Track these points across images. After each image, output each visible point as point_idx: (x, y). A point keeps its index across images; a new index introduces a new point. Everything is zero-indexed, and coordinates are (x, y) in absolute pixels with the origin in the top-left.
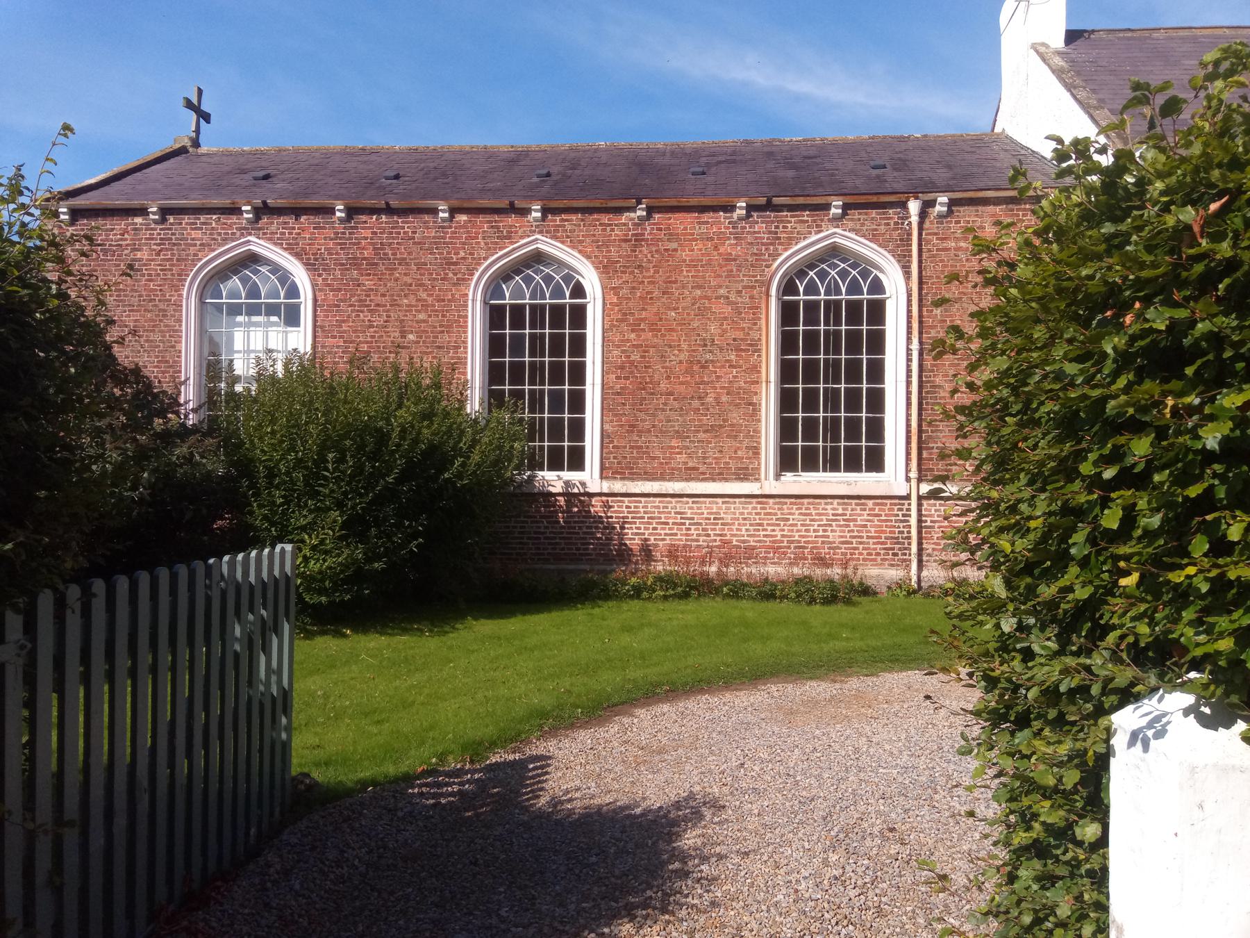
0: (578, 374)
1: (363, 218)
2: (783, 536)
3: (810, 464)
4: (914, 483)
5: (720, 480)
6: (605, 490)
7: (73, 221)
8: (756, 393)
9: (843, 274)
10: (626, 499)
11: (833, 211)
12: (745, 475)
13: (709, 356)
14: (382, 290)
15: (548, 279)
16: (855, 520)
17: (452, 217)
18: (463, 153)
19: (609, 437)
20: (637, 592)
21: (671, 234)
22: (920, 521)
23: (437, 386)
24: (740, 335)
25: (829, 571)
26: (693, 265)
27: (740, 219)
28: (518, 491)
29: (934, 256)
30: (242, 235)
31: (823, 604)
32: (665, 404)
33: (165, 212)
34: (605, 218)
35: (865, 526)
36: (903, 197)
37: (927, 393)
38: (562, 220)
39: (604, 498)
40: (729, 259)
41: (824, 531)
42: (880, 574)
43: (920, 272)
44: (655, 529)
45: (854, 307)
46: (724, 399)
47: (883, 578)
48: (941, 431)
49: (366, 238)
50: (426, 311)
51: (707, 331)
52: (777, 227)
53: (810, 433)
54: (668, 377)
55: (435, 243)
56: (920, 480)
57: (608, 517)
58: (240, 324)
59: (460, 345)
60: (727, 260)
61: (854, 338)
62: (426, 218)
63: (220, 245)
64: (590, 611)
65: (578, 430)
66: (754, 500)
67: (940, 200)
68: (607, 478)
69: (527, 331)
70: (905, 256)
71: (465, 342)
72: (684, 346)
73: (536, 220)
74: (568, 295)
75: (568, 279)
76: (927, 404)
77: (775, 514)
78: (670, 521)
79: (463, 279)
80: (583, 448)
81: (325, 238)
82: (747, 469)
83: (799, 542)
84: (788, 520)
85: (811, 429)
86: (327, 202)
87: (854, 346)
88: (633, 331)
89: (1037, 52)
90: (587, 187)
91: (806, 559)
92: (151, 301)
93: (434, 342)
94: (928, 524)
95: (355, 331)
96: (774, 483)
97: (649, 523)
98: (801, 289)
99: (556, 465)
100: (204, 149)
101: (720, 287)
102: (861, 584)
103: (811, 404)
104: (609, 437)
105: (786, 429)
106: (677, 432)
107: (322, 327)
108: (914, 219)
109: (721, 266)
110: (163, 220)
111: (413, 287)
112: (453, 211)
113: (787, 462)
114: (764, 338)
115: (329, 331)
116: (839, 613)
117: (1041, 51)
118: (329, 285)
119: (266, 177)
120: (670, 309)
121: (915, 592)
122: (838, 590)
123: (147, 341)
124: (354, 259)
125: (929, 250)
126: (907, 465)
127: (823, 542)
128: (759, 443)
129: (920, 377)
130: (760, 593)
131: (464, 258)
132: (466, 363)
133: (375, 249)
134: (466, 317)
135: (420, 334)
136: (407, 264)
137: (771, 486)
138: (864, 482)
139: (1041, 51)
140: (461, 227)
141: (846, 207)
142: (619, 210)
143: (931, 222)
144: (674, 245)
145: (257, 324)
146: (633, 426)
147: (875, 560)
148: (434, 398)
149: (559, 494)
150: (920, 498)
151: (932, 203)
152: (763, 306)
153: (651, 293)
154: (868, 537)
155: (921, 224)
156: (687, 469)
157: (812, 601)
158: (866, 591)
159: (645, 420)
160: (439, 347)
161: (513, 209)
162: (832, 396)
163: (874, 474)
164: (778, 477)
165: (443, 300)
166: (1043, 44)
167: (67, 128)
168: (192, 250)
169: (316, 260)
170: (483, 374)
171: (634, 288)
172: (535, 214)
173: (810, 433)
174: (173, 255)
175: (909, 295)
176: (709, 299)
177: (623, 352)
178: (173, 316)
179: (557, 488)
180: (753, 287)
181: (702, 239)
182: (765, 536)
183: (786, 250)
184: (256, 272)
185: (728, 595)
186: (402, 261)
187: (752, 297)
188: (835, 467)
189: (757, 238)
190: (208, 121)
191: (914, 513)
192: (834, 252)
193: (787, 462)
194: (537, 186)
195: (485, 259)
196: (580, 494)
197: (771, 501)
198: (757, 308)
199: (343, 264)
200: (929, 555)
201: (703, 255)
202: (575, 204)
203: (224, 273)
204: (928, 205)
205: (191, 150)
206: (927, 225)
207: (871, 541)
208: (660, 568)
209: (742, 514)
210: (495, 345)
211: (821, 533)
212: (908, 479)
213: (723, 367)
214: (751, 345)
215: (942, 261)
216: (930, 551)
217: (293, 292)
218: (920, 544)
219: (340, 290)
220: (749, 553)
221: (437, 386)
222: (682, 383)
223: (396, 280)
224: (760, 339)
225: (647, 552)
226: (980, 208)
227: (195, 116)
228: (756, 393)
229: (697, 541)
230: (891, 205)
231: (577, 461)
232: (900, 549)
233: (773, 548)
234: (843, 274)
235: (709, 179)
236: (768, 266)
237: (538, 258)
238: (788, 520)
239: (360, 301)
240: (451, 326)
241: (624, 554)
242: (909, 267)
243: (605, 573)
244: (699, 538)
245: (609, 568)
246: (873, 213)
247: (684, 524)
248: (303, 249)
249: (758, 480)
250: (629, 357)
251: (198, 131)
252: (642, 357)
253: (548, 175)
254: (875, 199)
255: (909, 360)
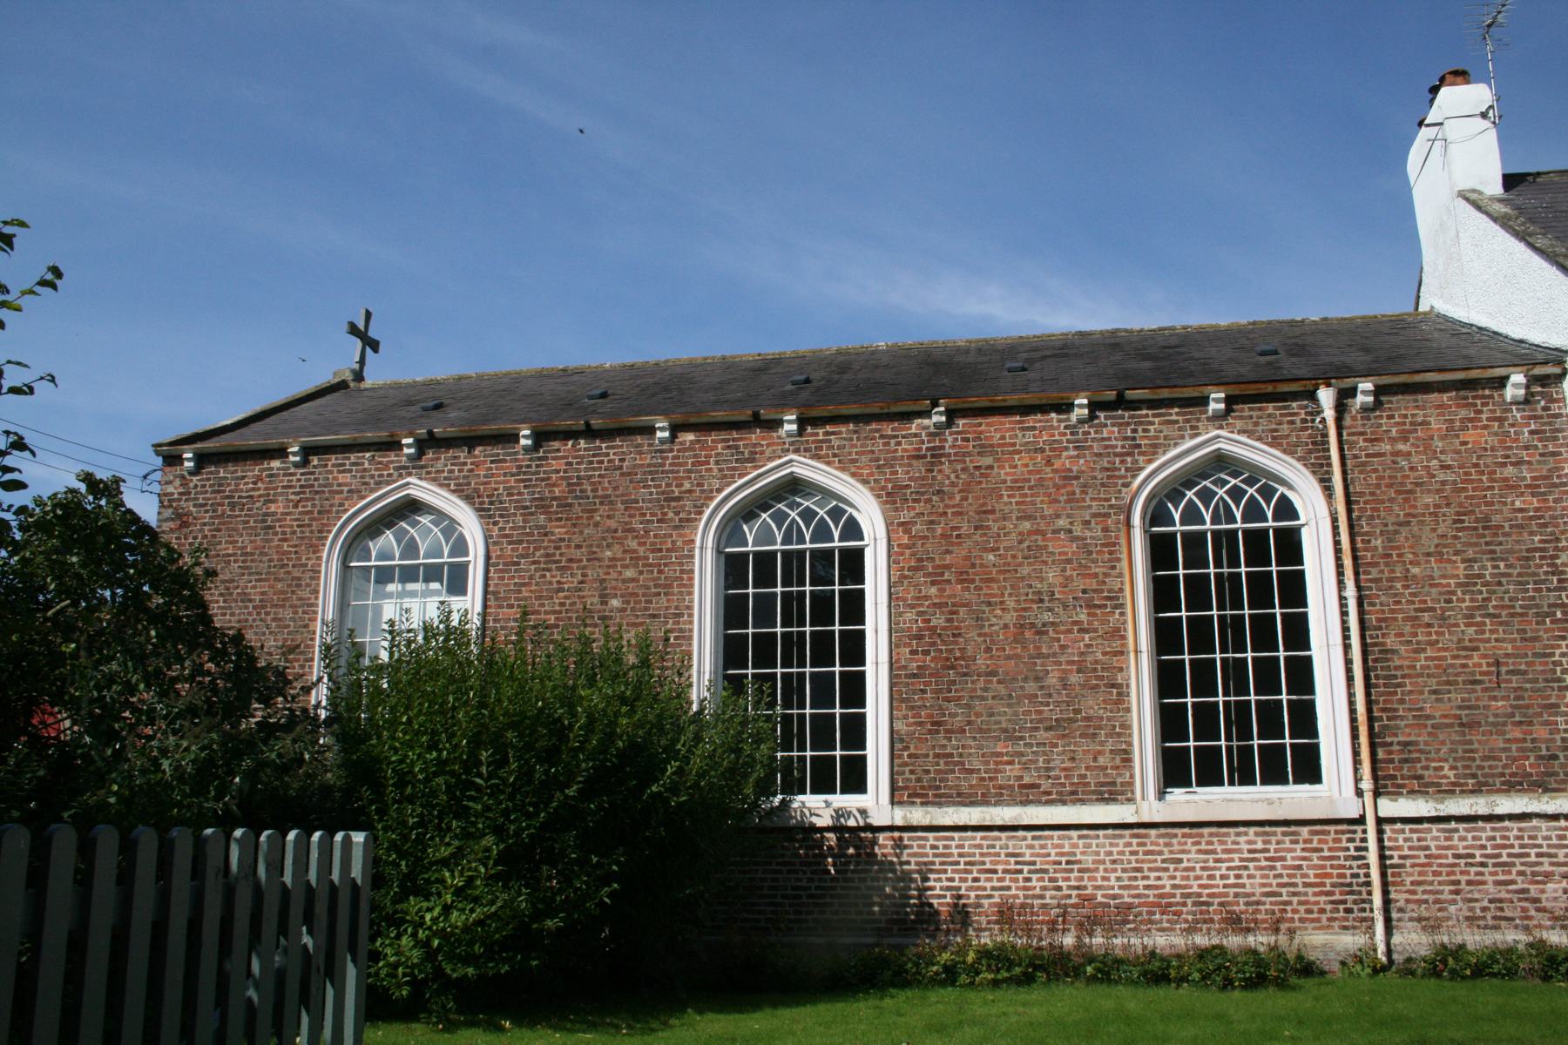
0: (855, 649)
1: (556, 444)
2: (1174, 887)
3: (1210, 777)
4: (1368, 797)
5: (1074, 802)
6: (899, 822)
7: (197, 471)
8: (1121, 670)
9: (1236, 494)
10: (930, 835)
11: (1213, 406)
12: (1113, 792)
13: (1047, 617)
14: (577, 539)
15: (808, 515)
16: (1283, 859)
17: (673, 436)
18: (692, 365)
19: (902, 740)
20: (950, 975)
21: (982, 446)
22: (1382, 857)
23: (645, 663)
24: (1092, 584)
25: (1251, 939)
26: (1017, 486)
27: (1081, 422)
28: (767, 823)
29: (1364, 464)
30: (401, 476)
31: (1244, 988)
32: (985, 690)
33: (308, 451)
34: (888, 428)
35: (1299, 867)
36: (1309, 385)
37: (1375, 661)
38: (827, 433)
39: (896, 834)
40: (1068, 477)
41: (1238, 877)
42: (1329, 942)
43: (1346, 487)
44: (976, 880)
45: (1256, 541)
46: (1074, 679)
47: (1332, 948)
48: (1402, 718)
49: (558, 472)
50: (636, 566)
51: (1042, 579)
52: (1134, 431)
53: (1207, 727)
54: (988, 650)
55: (650, 473)
56: (1377, 794)
57: (902, 863)
58: (390, 596)
59: (682, 612)
60: (1066, 478)
61: (1260, 584)
62: (639, 440)
63: (373, 491)
64: (877, 1002)
65: (855, 731)
66: (1127, 832)
67: (1361, 386)
68: (901, 803)
69: (779, 589)
70: (1322, 465)
71: (690, 608)
72: (1010, 603)
73: (789, 435)
74: (836, 535)
75: (836, 514)
76: (1377, 677)
77: (1160, 853)
78: (1000, 867)
79: (688, 520)
80: (863, 758)
81: (505, 475)
82: (1114, 784)
83: (1200, 895)
84: (1180, 861)
85: (1207, 721)
86: (507, 426)
87: (1261, 594)
88: (933, 583)
89: (1467, 199)
90: (855, 393)
91: (1212, 921)
92: (283, 566)
93: (646, 609)
94: (1396, 861)
95: (539, 598)
96: (1156, 804)
97: (967, 872)
98: (1177, 517)
99: (823, 785)
100: (368, 383)
101: (1058, 516)
102: (1300, 958)
103: (1204, 685)
104: (902, 740)
105: (1170, 723)
106: (1005, 731)
107: (495, 593)
108: (1329, 414)
109: (1058, 487)
110: (305, 462)
111: (620, 534)
112: (675, 429)
113: (1174, 773)
114: (1127, 588)
115: (505, 599)
116: (1270, 1001)
117: (1473, 200)
118: (506, 536)
119: (438, 407)
120: (986, 550)
121: (1384, 969)
122: (1267, 966)
123: (274, 620)
124: (541, 499)
125: (1355, 457)
126: (1356, 770)
127: (1236, 895)
128: (1130, 744)
129: (1363, 637)
130: (1145, 974)
131: (690, 491)
132: (691, 638)
133: (569, 485)
134: (692, 571)
135: (628, 597)
136: (611, 503)
137: (1149, 807)
138: (1292, 799)
139: (1473, 200)
140: (685, 450)
141: (1230, 401)
142: (908, 416)
143: (1354, 418)
144: (988, 461)
145: (413, 594)
146: (939, 724)
147: (1318, 920)
148: (646, 683)
149: (828, 829)
150: (1380, 821)
151: (1352, 392)
152: (1123, 541)
153: (958, 528)
154: (1306, 885)
155: (1339, 421)
156: (1022, 786)
157: (1228, 984)
158: (1307, 969)
159: (956, 715)
160: (654, 616)
161: (757, 422)
162: (1236, 671)
163: (1307, 787)
164: (1161, 795)
165: (660, 550)
166: (1474, 191)
167: (57, 272)
168: (337, 499)
169: (491, 503)
170: (716, 653)
171: (932, 522)
172: (787, 427)
173: (1207, 727)
174: (314, 506)
175: (1334, 520)
176: (1043, 533)
177: (920, 614)
178: (308, 585)
179: (824, 821)
180: (1107, 515)
181: (1028, 451)
182: (1147, 887)
183: (1150, 461)
184: (414, 524)
185: (1093, 979)
186: (605, 500)
187: (1106, 530)
188: (1247, 780)
189: (1106, 447)
190: (376, 350)
191: (1372, 844)
192: (1221, 463)
193: (1174, 773)
194: (792, 393)
195: (719, 491)
196: (859, 829)
197: (1153, 832)
198: (1114, 544)
199: (526, 508)
200: (1401, 910)
201: (1030, 472)
202: (846, 410)
203: (374, 527)
204: (1345, 395)
205: (352, 384)
206: (1347, 421)
207: (1310, 890)
208: (985, 939)
209: (1110, 853)
210: (732, 612)
211: (1232, 881)
212: (1359, 793)
213: (1070, 631)
214: (1109, 598)
215: (1375, 471)
216: (1401, 904)
217: (460, 547)
218: (1385, 892)
219: (521, 542)
220: (1120, 916)
221: (645, 663)
222: (1009, 658)
223: (597, 525)
224: (1121, 590)
225: (962, 915)
226: (1420, 397)
227: (359, 344)
228: (1121, 670)
229: (1042, 897)
230: (1295, 396)
231: (855, 780)
232: (1355, 902)
233: (1159, 905)
234: (1236, 494)
235: (1031, 375)
236: (1126, 485)
237: (794, 486)
238: (1180, 861)
239: (547, 555)
240: (671, 586)
241: (927, 917)
242: (1329, 480)
243: (901, 948)
244: (1041, 892)
245: (905, 941)
246: (1270, 408)
247: (1021, 872)
248: (476, 490)
249: (1131, 800)
250: (929, 621)
251: (362, 362)
252: (950, 620)
253: (808, 381)
254: (1270, 388)
255: (1344, 614)
